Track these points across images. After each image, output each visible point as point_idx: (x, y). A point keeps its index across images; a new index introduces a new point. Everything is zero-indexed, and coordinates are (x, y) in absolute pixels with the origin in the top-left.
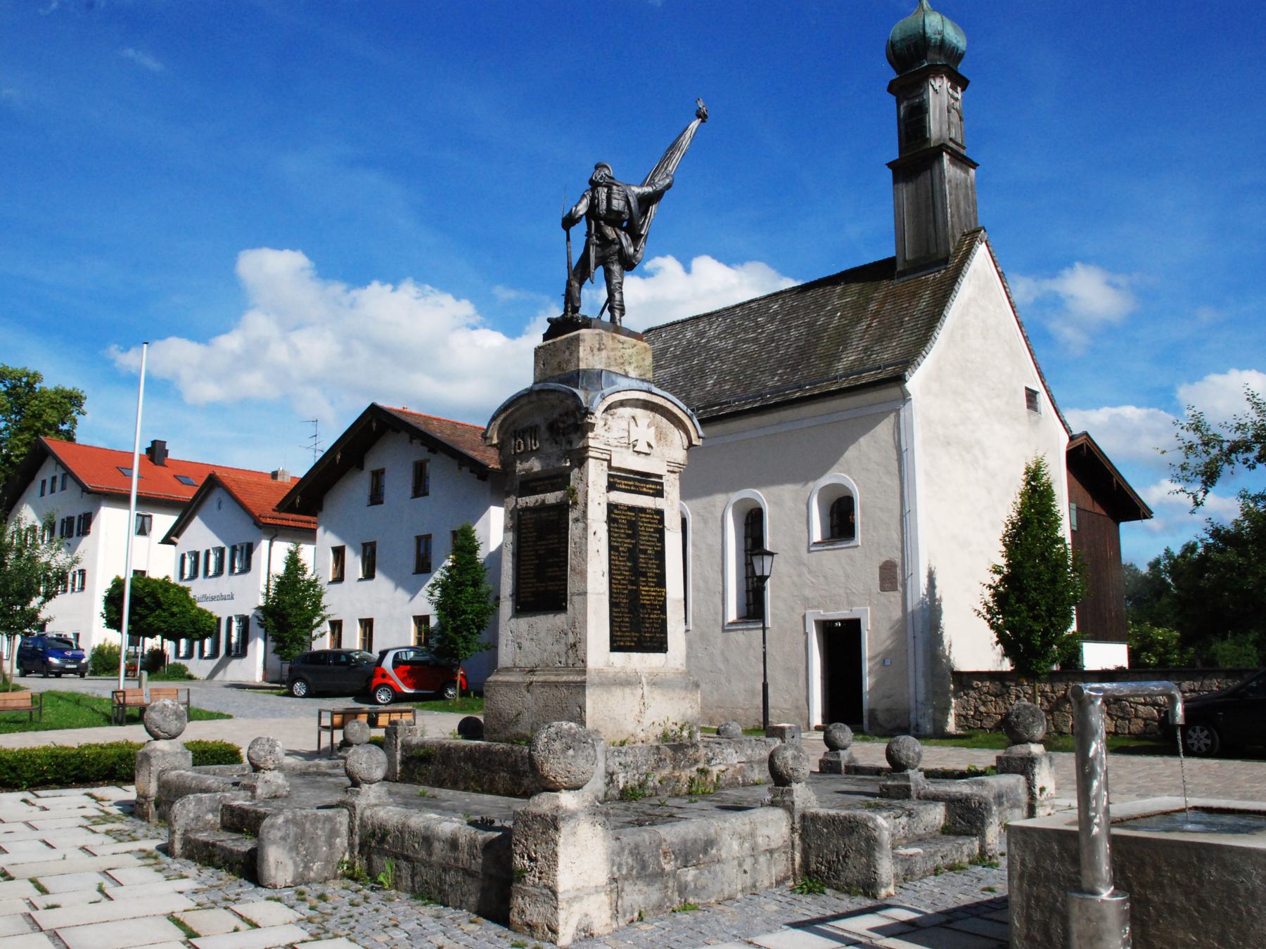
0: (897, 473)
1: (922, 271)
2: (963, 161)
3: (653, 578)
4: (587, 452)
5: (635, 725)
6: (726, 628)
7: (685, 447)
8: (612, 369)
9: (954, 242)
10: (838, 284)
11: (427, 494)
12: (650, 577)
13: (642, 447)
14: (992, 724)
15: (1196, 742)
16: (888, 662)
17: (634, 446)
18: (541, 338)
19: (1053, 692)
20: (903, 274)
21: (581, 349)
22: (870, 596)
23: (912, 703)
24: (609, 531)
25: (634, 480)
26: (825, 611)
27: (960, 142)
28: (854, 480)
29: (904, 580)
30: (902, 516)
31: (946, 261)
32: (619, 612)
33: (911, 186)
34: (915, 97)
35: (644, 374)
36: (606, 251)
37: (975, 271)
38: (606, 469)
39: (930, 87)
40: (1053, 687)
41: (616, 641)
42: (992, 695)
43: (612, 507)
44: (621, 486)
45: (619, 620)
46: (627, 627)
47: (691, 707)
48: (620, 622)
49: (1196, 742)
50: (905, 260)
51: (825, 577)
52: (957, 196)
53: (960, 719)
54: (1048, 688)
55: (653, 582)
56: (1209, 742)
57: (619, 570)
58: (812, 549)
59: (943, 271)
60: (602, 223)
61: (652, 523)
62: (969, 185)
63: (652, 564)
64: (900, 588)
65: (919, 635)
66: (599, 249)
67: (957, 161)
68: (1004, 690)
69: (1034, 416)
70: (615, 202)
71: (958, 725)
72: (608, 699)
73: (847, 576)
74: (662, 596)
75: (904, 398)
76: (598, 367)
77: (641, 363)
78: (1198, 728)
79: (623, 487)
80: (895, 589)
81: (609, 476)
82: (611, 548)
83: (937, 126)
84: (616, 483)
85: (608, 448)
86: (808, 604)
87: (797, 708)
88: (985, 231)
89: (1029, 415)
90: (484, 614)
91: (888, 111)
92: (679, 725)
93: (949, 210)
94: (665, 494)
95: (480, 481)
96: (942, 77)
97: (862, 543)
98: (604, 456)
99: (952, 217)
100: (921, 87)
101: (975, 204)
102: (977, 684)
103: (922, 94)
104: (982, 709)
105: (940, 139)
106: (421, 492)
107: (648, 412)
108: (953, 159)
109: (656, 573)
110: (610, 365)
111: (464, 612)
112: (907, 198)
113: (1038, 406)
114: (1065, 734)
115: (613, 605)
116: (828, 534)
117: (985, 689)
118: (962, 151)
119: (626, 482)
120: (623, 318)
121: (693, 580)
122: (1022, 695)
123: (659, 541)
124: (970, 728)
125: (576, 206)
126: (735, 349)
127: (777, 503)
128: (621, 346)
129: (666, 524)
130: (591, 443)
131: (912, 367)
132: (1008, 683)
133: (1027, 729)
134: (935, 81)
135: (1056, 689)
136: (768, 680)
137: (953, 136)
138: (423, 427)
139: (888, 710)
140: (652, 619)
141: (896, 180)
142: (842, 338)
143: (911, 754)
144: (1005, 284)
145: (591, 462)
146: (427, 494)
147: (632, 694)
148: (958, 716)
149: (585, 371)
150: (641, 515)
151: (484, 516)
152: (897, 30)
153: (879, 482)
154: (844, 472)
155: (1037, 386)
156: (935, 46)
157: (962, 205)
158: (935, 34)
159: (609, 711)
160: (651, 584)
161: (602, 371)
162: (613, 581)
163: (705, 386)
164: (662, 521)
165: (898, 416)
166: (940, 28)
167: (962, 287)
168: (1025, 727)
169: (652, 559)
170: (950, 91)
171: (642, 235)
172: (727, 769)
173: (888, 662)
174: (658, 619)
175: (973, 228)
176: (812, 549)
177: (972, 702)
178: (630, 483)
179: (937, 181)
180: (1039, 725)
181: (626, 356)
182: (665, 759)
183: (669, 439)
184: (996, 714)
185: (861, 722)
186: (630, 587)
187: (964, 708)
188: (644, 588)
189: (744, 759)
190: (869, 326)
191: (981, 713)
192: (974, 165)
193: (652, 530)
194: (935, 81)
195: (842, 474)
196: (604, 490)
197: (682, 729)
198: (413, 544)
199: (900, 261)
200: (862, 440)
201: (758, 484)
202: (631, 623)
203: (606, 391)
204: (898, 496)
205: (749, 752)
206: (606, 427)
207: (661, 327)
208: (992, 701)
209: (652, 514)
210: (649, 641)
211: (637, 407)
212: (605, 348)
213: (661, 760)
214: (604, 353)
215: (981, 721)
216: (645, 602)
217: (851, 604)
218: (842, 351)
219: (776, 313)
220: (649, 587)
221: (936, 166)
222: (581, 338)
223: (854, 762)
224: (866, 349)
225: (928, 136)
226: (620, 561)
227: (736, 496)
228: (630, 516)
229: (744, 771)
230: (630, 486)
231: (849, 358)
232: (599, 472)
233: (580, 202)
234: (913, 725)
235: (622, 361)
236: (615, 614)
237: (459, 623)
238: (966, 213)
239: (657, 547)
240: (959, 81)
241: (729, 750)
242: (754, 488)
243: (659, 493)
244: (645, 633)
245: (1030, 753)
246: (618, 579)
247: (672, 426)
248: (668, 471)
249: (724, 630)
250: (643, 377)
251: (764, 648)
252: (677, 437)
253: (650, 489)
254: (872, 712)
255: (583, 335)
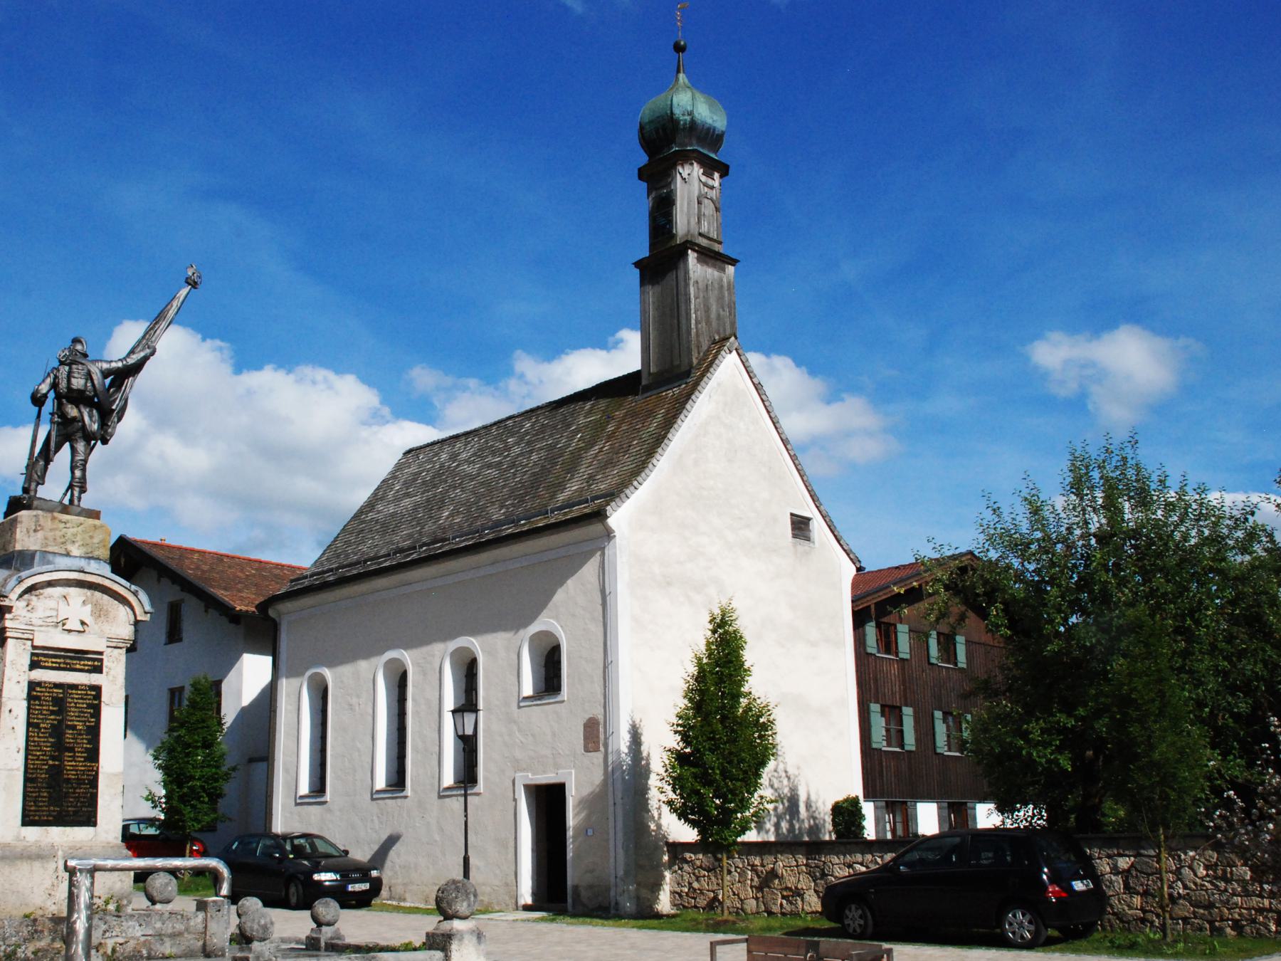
0: (601, 619)
1: (664, 386)
2: (711, 256)
3: (82, 752)
4: (5, 632)
5: (44, 897)
6: (375, 796)
7: (132, 622)
8: (50, 549)
9: (699, 353)
10: (590, 400)
11: (180, 640)
12: (78, 752)
13: (74, 624)
14: (705, 902)
15: (851, 922)
16: (590, 832)
17: (64, 625)
18: (2, 516)
19: (763, 865)
20: (647, 389)
21: (18, 530)
22: (574, 757)
23: (612, 879)
24: (29, 708)
25: (64, 657)
26: (533, 774)
27: (715, 237)
28: (561, 627)
29: (606, 739)
30: (605, 667)
31: (688, 374)
32: (35, 788)
33: (658, 288)
34: (663, 187)
35: (91, 552)
36: (69, 428)
37: (719, 384)
38: (30, 648)
39: (678, 174)
40: (762, 860)
41: (29, 816)
42: (704, 870)
43: (33, 685)
44: (46, 664)
45: (34, 795)
46: (44, 802)
47: (121, 880)
48: (36, 797)
49: (851, 922)
50: (650, 374)
51: (533, 735)
52: (706, 300)
53: (675, 897)
54: (757, 861)
55: (81, 757)
56: (862, 922)
57: (38, 746)
58: (522, 704)
59: (684, 386)
60: (64, 401)
61: (85, 699)
62: (725, 284)
63: (83, 739)
64: (602, 749)
65: (619, 801)
66: (61, 427)
67: (708, 260)
68: (717, 864)
69: (802, 545)
70: (74, 381)
71: (674, 904)
72: (11, 872)
73: (554, 734)
74: (92, 770)
75: (609, 536)
76: (33, 548)
77: (89, 541)
78: (853, 907)
79: (50, 664)
80: (597, 750)
81: (33, 654)
82: (29, 724)
83: (683, 222)
84: (41, 661)
85: (31, 628)
86: (518, 769)
87: (507, 885)
88: (736, 338)
89: (795, 545)
90: (216, 780)
91: (640, 201)
92: (103, 899)
93: (693, 316)
94: (105, 670)
95: (232, 625)
96: (692, 164)
97: (568, 697)
98: (26, 636)
99: (697, 322)
100: (669, 175)
101: (732, 306)
102: (691, 857)
103: (670, 183)
104: (696, 885)
105: (687, 235)
106: (177, 637)
107: (86, 590)
108: (703, 257)
109: (86, 748)
110: (47, 545)
111: (192, 778)
112: (654, 303)
113: (811, 534)
114: (774, 913)
115: (27, 780)
116: (543, 685)
117: (698, 863)
118: (717, 247)
119: (54, 660)
120: (83, 495)
121: (413, 740)
122: (733, 870)
123: (92, 716)
124: (684, 906)
125: (39, 386)
126: (479, 475)
127: (490, 653)
128: (63, 525)
129: (103, 699)
130: (8, 624)
131: (617, 500)
132: (719, 856)
133: (450, 905)
134: (683, 168)
135: (765, 862)
136: (469, 854)
137: (704, 229)
138: (173, 565)
139: (590, 887)
140: (79, 793)
141: (644, 281)
142: (572, 467)
143: (256, 927)
144: (764, 397)
145: (10, 642)
146: (180, 640)
147: (43, 867)
148: (673, 893)
149: (21, 552)
150: (70, 692)
151: (237, 666)
152: (648, 108)
153: (584, 629)
154: (552, 618)
155: (808, 510)
156: (684, 128)
157: (714, 308)
158: (683, 115)
159: (11, 884)
160: (80, 759)
161: (36, 551)
162: (30, 757)
163: (439, 519)
164: (98, 696)
165: (603, 555)
166: (689, 108)
167: (696, 406)
168: (447, 902)
169: (82, 735)
170: (704, 179)
171: (114, 410)
172: (126, 942)
173: (590, 832)
174: (86, 793)
175: (722, 336)
176: (522, 704)
177: (686, 877)
178: (58, 660)
179: (682, 284)
180: (463, 901)
181: (69, 535)
182: (42, 931)
183: (111, 615)
184: (708, 891)
185: (565, 901)
186: (51, 762)
187: (678, 884)
188: (70, 763)
189: (150, 932)
190: (601, 450)
191: (695, 890)
192: (733, 262)
193: (85, 706)
194: (683, 168)
195: (552, 621)
196: (26, 667)
197: (107, 903)
198: (165, 697)
199: (644, 376)
200: (569, 582)
201: (474, 632)
202: (50, 797)
203: (36, 569)
204: (602, 645)
205: (158, 925)
206: (29, 608)
207: (421, 448)
208: (704, 876)
209: (86, 690)
210: (74, 815)
211: (70, 586)
212: (42, 529)
213: (36, 931)
214: (40, 534)
215: (695, 898)
216: (70, 776)
217: (557, 766)
218: (569, 480)
219: (527, 433)
220: (76, 761)
221: (682, 265)
222: (19, 519)
223: (338, 938)
224: (591, 477)
225: (674, 232)
226: (39, 737)
227: (453, 645)
228: (57, 693)
229: (150, 943)
230: (60, 663)
231: (573, 487)
232: (20, 650)
233: (44, 381)
234: (613, 904)
235: (63, 540)
236: (29, 789)
237: (185, 790)
238: (719, 316)
239: (90, 722)
240: (711, 166)
241: (130, 923)
242: (470, 636)
243: (98, 669)
244: (68, 807)
245: (452, 929)
246: (36, 755)
247: (116, 602)
248: (108, 647)
249: (440, 797)
250: (90, 555)
251: (466, 816)
252: (123, 613)
253: (84, 665)
254: (576, 888)
255: (21, 516)
